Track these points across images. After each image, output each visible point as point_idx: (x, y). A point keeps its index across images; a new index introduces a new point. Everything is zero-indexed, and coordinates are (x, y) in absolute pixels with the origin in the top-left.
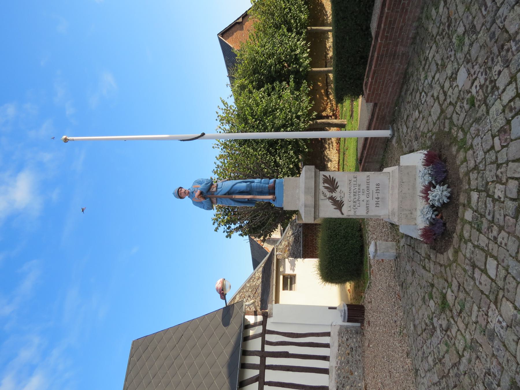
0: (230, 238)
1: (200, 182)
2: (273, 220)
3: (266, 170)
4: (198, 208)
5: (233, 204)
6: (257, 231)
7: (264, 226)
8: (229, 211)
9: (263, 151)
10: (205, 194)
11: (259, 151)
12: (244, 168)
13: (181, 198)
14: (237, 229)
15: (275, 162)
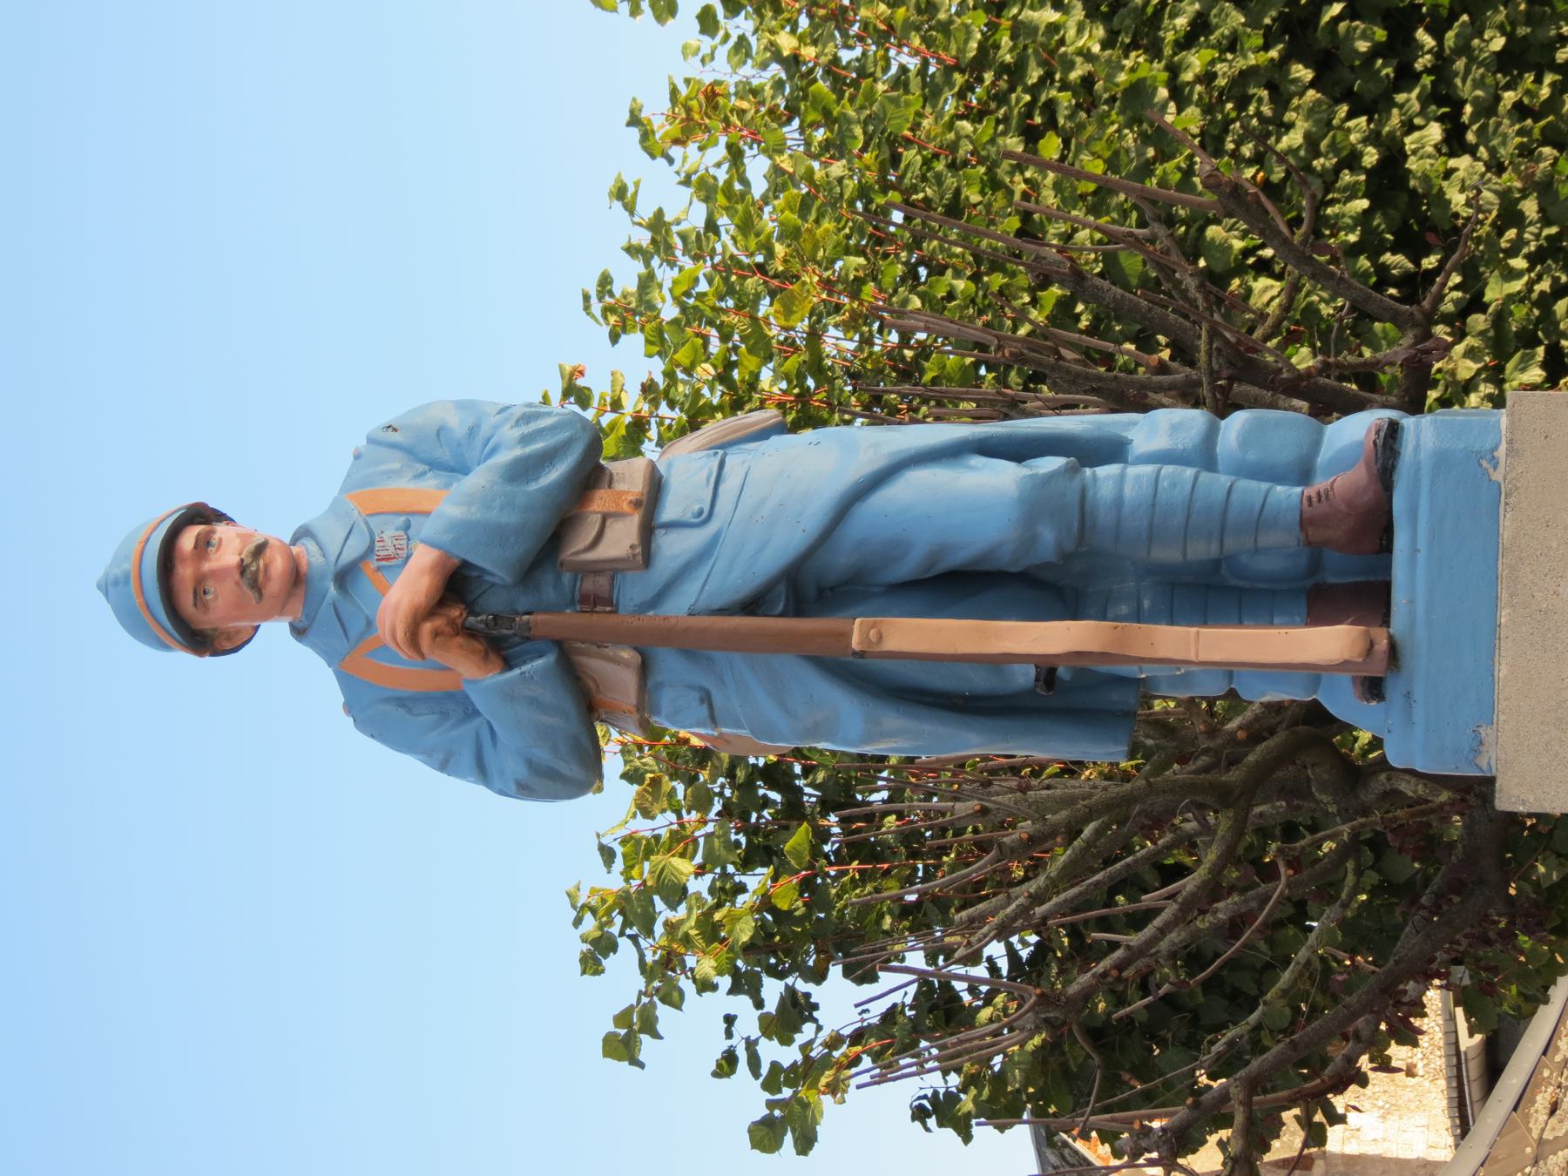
0: (806, 1143)
1: (435, 450)
2: (1355, 935)
3: (1266, 291)
4: (408, 775)
5: (849, 727)
6: (1145, 1070)
7: (1243, 1002)
8: (794, 810)
9: (1233, 44)
10: (496, 602)
11: (1188, 41)
12: (984, 264)
13: (201, 641)
14: (888, 1042)
15: (1389, 179)
